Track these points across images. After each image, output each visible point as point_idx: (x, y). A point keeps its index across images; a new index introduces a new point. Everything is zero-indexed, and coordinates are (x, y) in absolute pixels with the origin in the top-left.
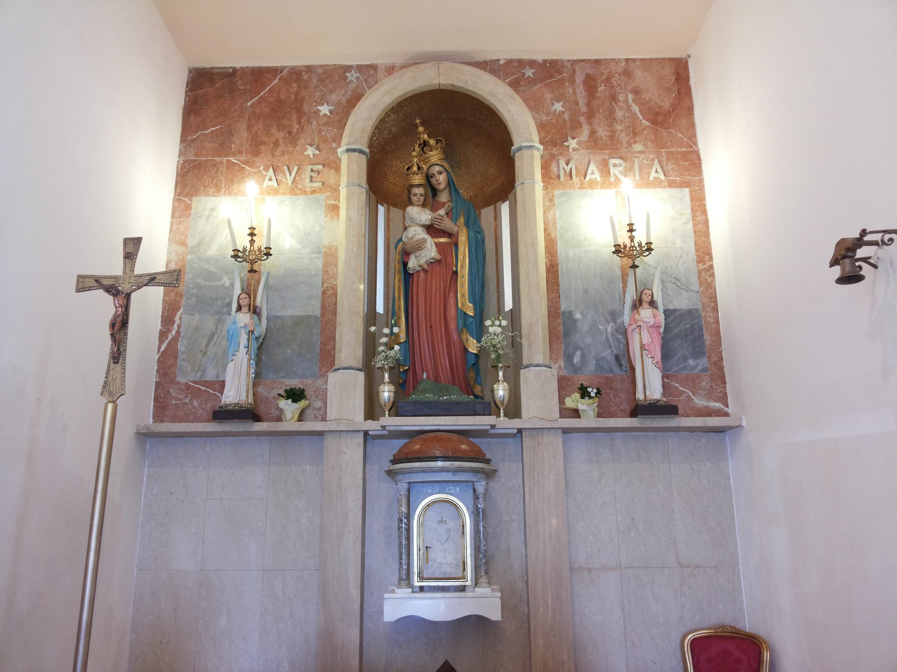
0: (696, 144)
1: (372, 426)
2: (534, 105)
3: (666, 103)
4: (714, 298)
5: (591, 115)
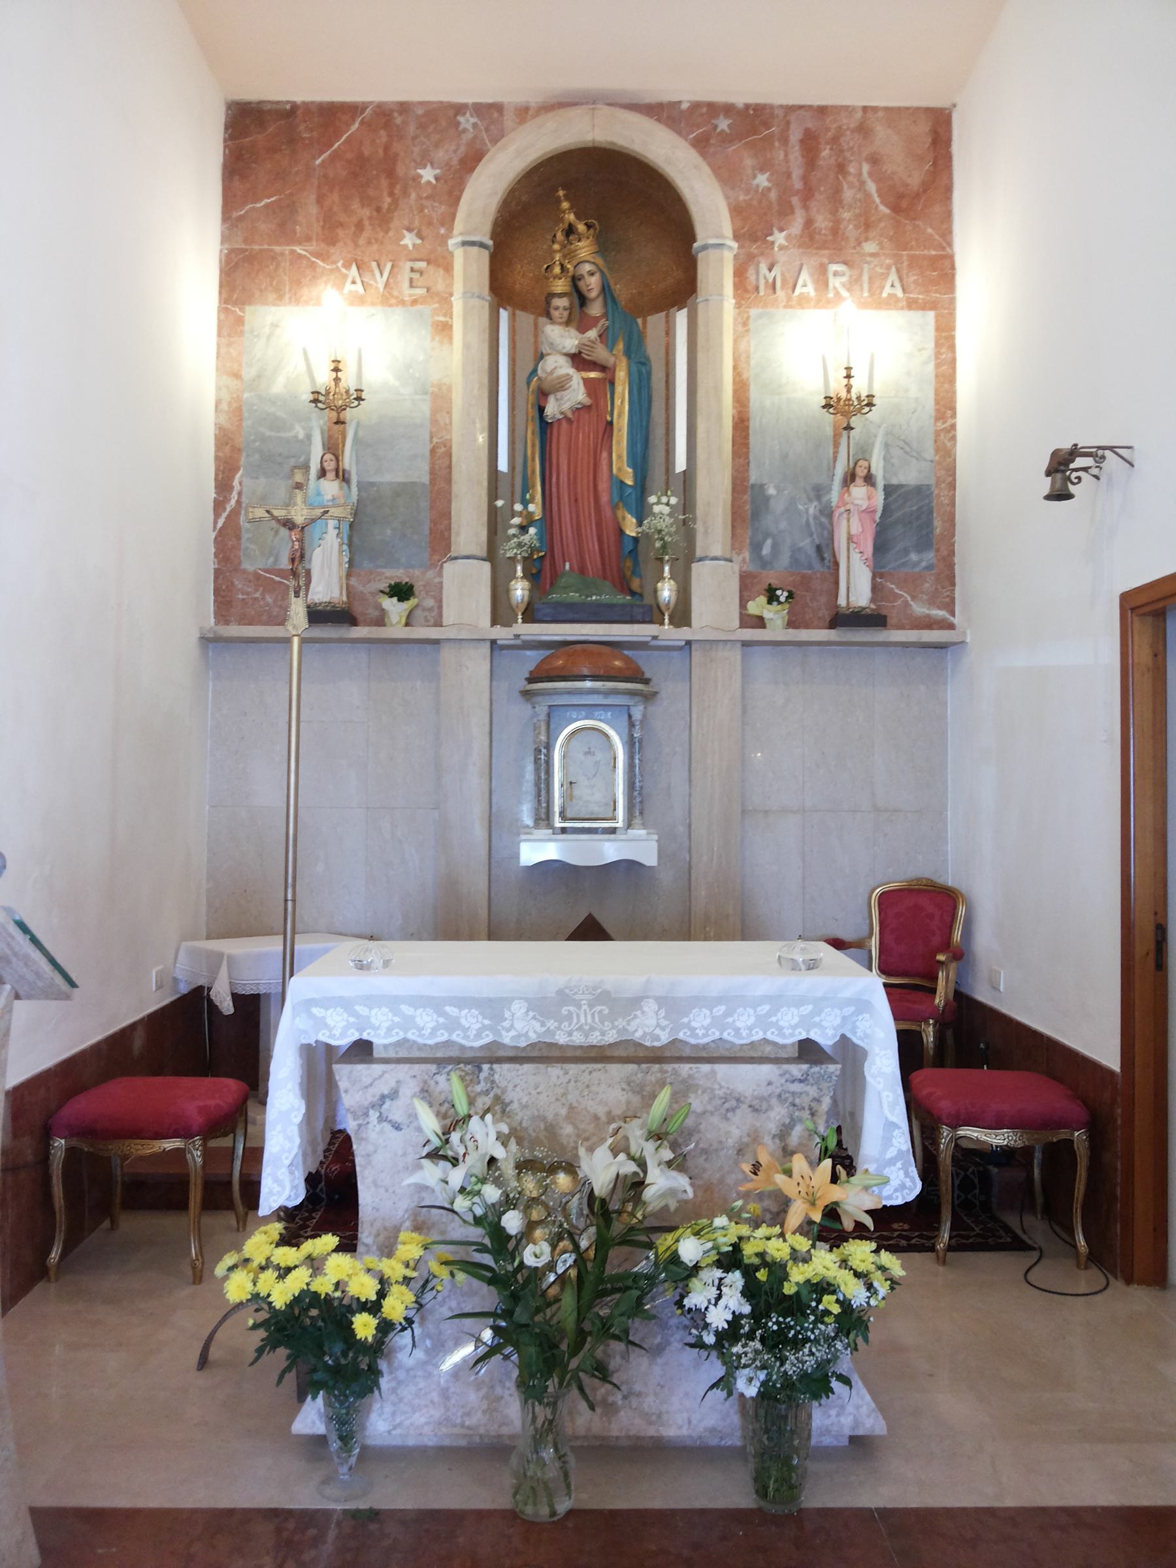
0: (950, 245)
1: (501, 633)
2: (727, 176)
3: (915, 180)
4: (952, 471)
5: (808, 194)
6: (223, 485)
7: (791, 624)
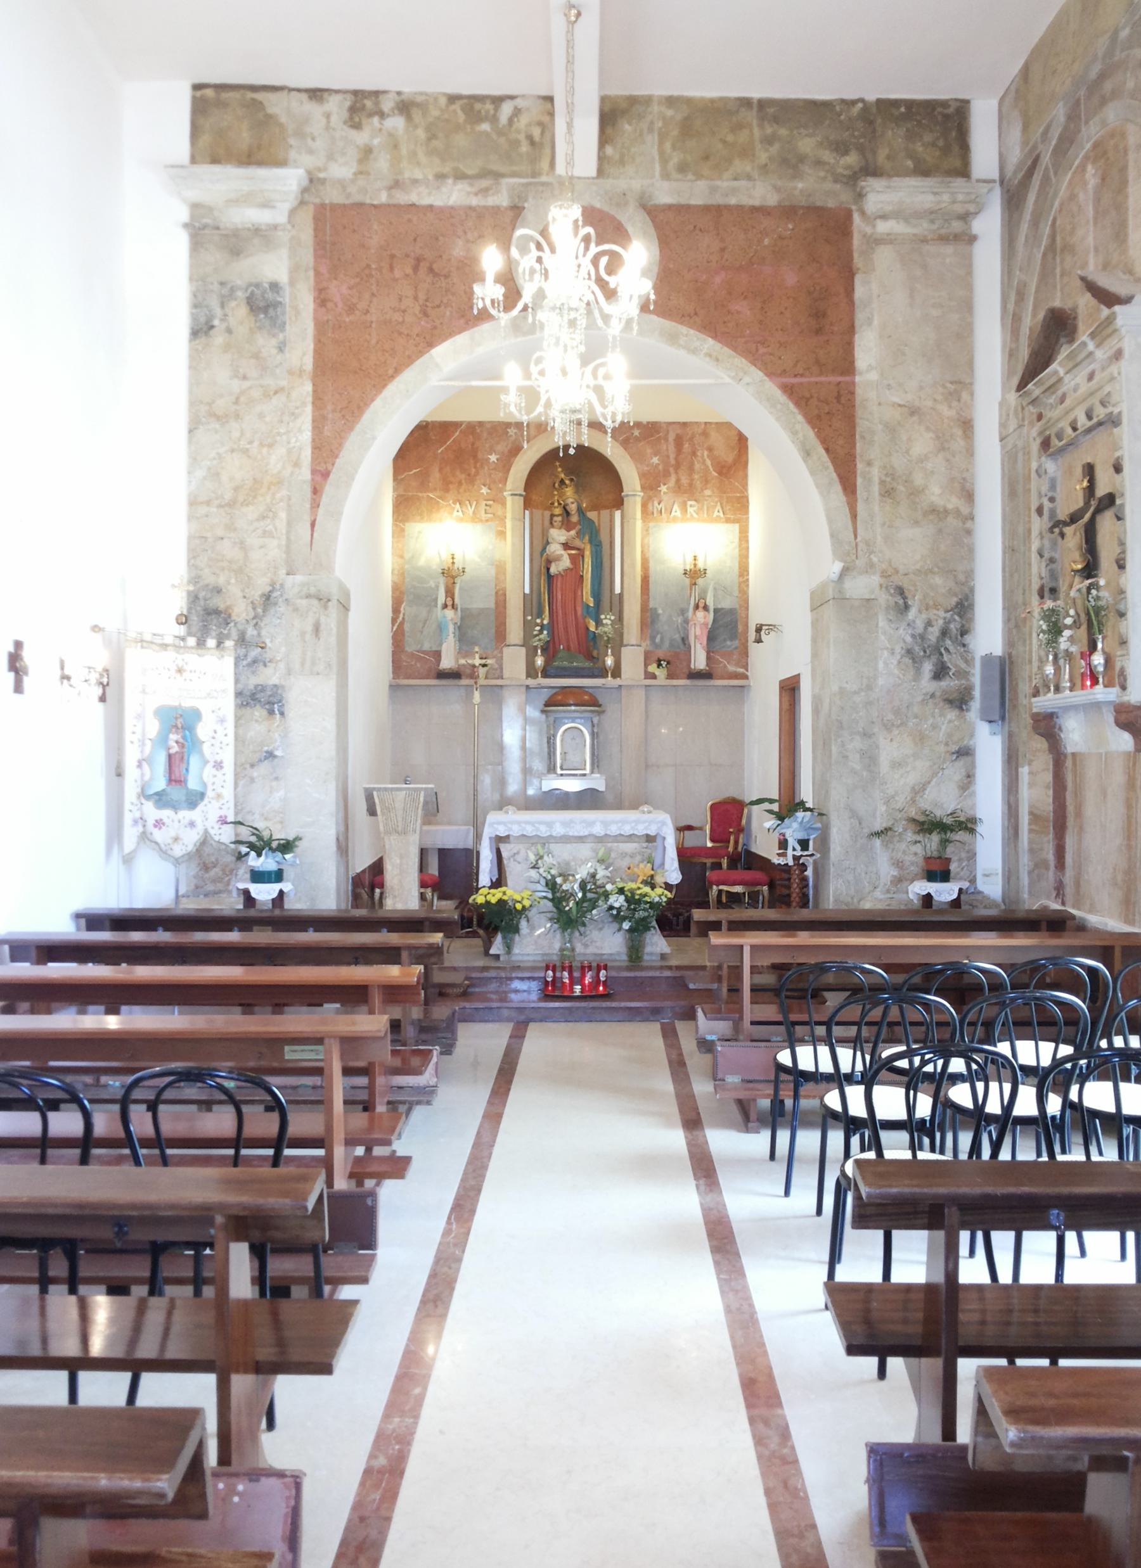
0: (746, 490)
1: (531, 682)
2: (638, 458)
3: (729, 457)
4: (747, 601)
5: (677, 466)
6: (396, 610)
7: (670, 676)
